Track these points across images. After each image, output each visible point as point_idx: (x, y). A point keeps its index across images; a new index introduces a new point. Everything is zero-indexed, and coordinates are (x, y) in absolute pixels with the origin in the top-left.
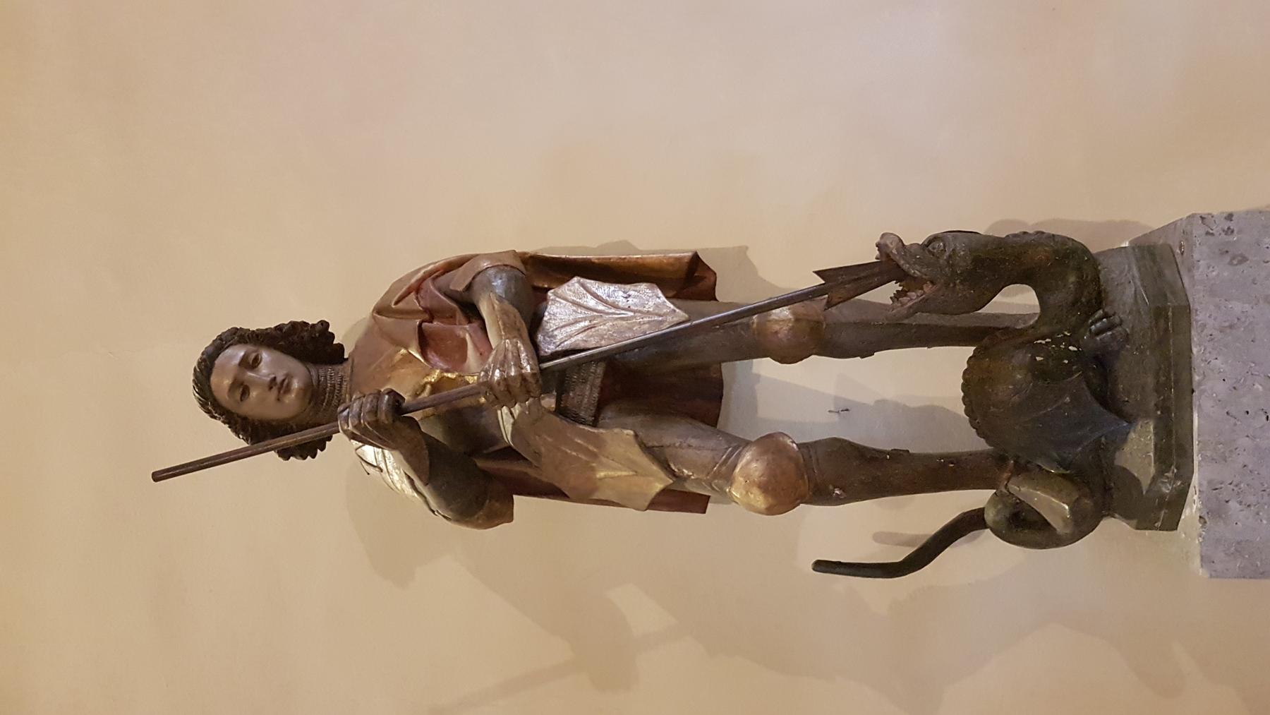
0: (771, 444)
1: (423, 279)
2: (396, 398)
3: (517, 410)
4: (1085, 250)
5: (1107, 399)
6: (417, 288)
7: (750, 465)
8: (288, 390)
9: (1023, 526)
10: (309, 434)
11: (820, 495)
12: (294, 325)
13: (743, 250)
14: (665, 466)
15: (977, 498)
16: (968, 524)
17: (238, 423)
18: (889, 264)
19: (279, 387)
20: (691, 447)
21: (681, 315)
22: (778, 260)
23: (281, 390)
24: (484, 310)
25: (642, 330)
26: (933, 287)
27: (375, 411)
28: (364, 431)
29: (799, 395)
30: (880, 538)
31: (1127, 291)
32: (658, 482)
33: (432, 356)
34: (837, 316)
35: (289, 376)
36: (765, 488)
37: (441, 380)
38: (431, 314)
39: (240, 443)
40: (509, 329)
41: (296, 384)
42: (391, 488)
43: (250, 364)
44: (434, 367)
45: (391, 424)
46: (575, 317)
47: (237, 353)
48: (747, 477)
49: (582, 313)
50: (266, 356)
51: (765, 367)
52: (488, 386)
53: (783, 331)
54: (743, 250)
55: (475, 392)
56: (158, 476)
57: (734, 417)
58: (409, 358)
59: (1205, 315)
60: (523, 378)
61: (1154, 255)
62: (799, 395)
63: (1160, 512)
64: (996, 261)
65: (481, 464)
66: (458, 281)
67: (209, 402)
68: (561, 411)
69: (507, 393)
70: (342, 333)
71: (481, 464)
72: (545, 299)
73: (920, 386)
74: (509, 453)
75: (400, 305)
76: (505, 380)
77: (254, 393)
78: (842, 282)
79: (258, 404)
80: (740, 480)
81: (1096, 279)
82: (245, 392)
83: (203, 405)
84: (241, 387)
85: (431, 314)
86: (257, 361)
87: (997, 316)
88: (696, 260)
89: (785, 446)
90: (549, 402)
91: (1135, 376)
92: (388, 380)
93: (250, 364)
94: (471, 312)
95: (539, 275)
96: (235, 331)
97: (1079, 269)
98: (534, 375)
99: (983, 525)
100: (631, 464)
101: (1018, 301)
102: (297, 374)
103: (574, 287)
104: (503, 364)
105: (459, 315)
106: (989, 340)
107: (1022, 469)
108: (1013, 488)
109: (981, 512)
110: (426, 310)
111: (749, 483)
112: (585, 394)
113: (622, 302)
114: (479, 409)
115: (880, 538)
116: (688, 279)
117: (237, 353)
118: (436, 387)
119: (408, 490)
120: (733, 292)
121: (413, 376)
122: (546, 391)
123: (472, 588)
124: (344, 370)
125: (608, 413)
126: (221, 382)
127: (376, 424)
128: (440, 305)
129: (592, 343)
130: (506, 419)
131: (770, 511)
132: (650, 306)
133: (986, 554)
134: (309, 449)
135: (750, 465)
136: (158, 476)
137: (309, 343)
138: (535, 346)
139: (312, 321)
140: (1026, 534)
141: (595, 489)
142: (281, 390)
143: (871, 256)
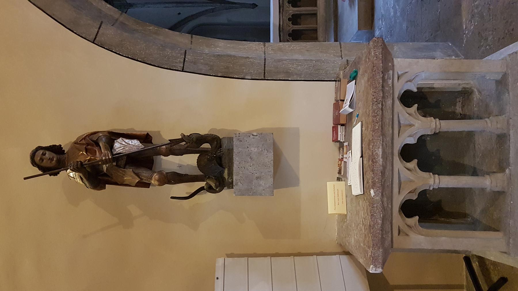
0: (160, 173)
1: (86, 137)
2: (81, 162)
3: (107, 165)
4: (219, 137)
5: (221, 165)
6: (84, 138)
7: (156, 176)
8: (53, 160)
9: (210, 189)
10: (57, 171)
11: (169, 182)
12: (53, 145)
13: (159, 132)
14: (139, 176)
15: (203, 184)
16: (202, 189)
17: (40, 168)
18: (184, 138)
19: (51, 160)
20: (145, 173)
21: (143, 147)
22: (168, 131)
23: (50, 160)
24: (101, 145)
25: (135, 150)
26: (192, 143)
27: (77, 165)
28: (75, 169)
29: (172, 163)
30: (187, 193)
31: (225, 145)
32: (137, 180)
33: (88, 154)
34: (176, 147)
35: (53, 158)
36: (158, 181)
37: (90, 159)
38: (88, 144)
39: (41, 173)
40: (106, 149)
41: (55, 159)
42: (77, 182)
43: (44, 154)
44: (89, 156)
45: (79, 168)
46: (120, 146)
47: (41, 152)
48: (155, 178)
49: (122, 146)
50: (47, 152)
51: (162, 157)
52: (101, 160)
53: (164, 151)
54: (159, 132)
55: (99, 161)
56: (25, 179)
57: (156, 167)
58: (83, 154)
59: (235, 150)
60: (109, 158)
61: (231, 139)
62: (172, 163)
63: (230, 185)
64: (200, 139)
65: (100, 177)
66: (95, 138)
67: (34, 163)
68: (117, 165)
69: (106, 162)
70: (66, 149)
71: (100, 177)
72: (114, 142)
73: (189, 161)
74: (105, 175)
75: (81, 142)
76: (106, 159)
77: (45, 161)
78: (173, 142)
79: (46, 163)
80: (153, 179)
81: (220, 143)
82: (43, 161)
83: (32, 164)
84: (42, 160)
85: (88, 144)
86: (45, 154)
87: (204, 148)
88: (148, 133)
89: (163, 173)
90: (115, 164)
91: (225, 161)
92: (77, 159)
93: (44, 154)
94: (98, 145)
95: (113, 136)
96: (39, 147)
97: (217, 141)
98: (343, 218)
99: (204, 189)
100: (131, 176)
101: (206, 146)
102: (55, 157)
103: (120, 140)
104: (105, 156)
105: (95, 145)
106: (203, 153)
107: (209, 178)
108: (209, 182)
109: (204, 187)
110: (87, 144)
111: (155, 180)
112: (122, 162)
113: (131, 144)
114: (99, 165)
115: (187, 193)
116: (145, 138)
117: (41, 152)
118: (89, 160)
119: (81, 183)
120: (156, 141)
121: (83, 157)
122: (114, 162)
123: (94, 205)
124: (66, 156)
125: (127, 166)
126: (37, 159)
127: (77, 168)
128: (90, 142)
129: (124, 152)
130: (105, 167)
131: (159, 185)
132: (137, 145)
133: (207, 197)
134: (56, 174)
135: (156, 176)
136: (25, 179)
137: (56, 149)
138: (112, 152)
139: (57, 145)
140: (211, 191)
141: (124, 182)
142: (50, 160)
143: (180, 137)
